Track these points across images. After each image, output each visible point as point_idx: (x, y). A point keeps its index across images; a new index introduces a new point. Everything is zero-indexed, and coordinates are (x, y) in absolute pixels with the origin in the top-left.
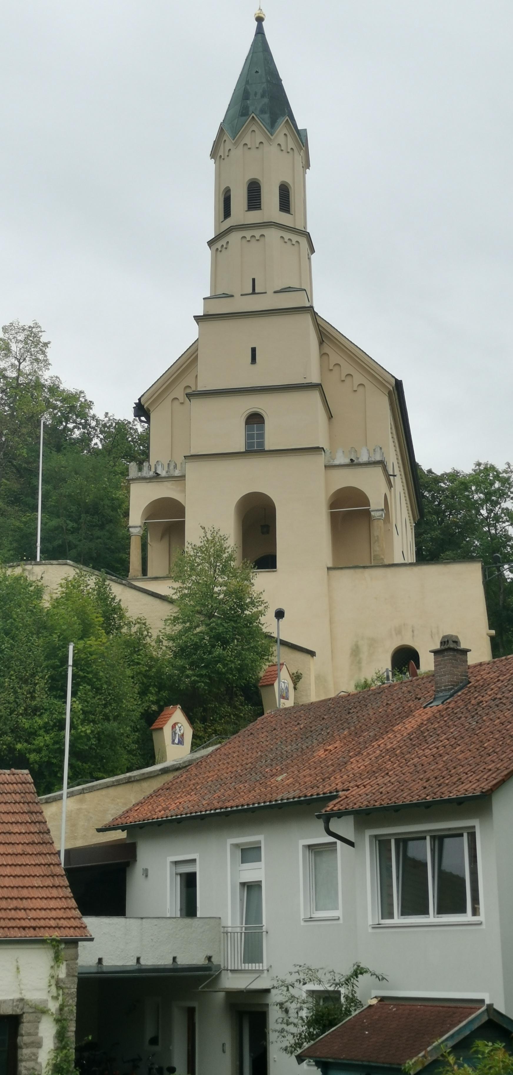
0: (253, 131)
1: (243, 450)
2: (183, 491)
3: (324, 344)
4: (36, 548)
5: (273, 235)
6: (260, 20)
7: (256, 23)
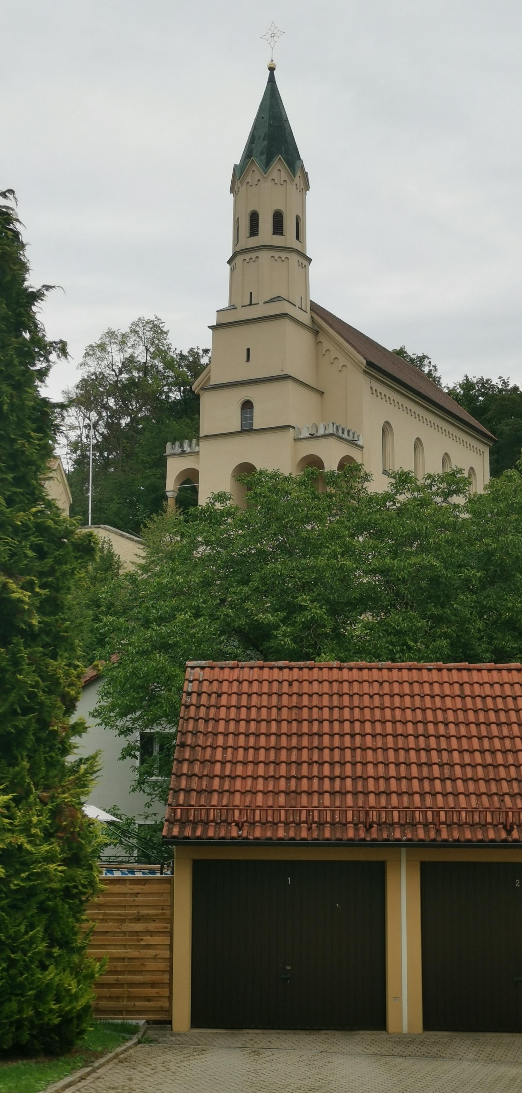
0: (254, 171)
1: (239, 430)
2: (199, 463)
3: (320, 334)
4: (88, 514)
5: (265, 256)
6: (272, 69)
7: (269, 72)
